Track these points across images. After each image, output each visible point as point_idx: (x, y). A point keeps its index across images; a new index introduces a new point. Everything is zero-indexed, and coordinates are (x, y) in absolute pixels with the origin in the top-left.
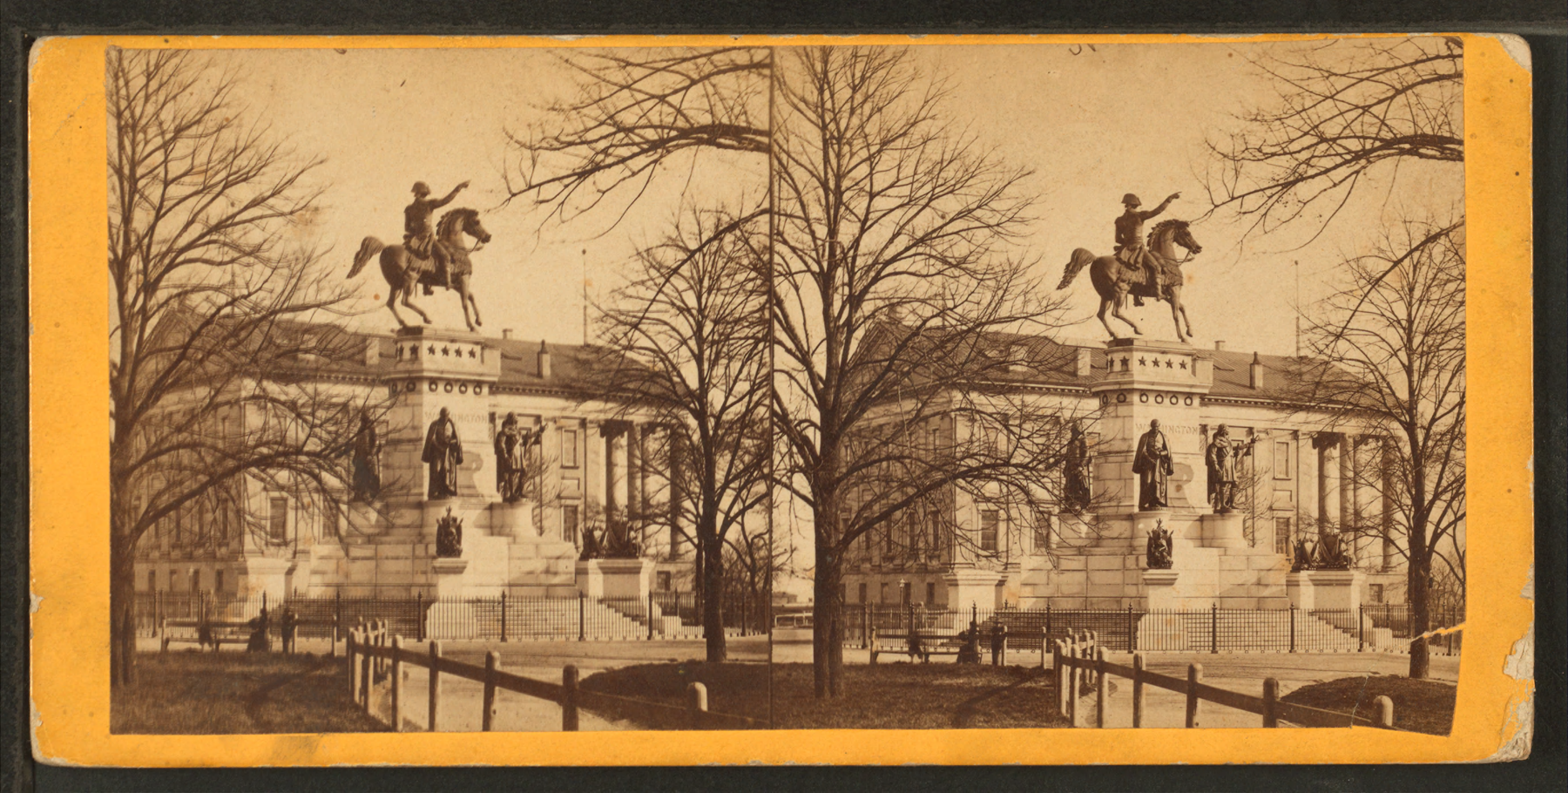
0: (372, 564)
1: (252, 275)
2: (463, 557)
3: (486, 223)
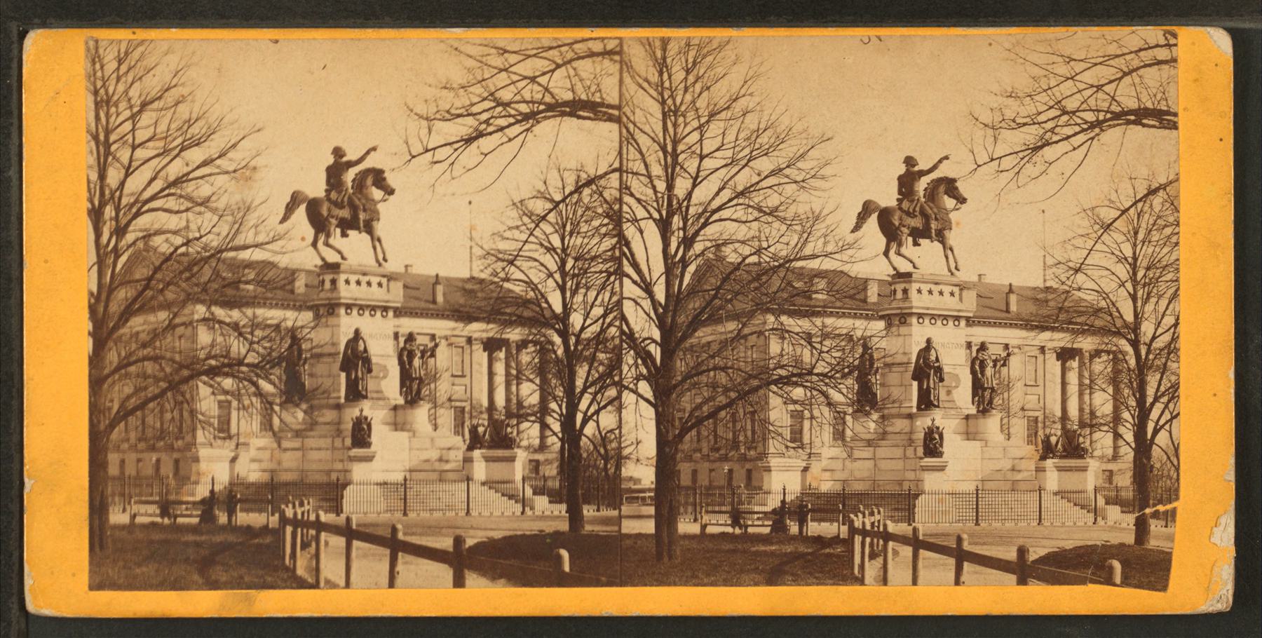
0: (299, 454)
1: (202, 221)
2: (373, 448)
3: (391, 179)
